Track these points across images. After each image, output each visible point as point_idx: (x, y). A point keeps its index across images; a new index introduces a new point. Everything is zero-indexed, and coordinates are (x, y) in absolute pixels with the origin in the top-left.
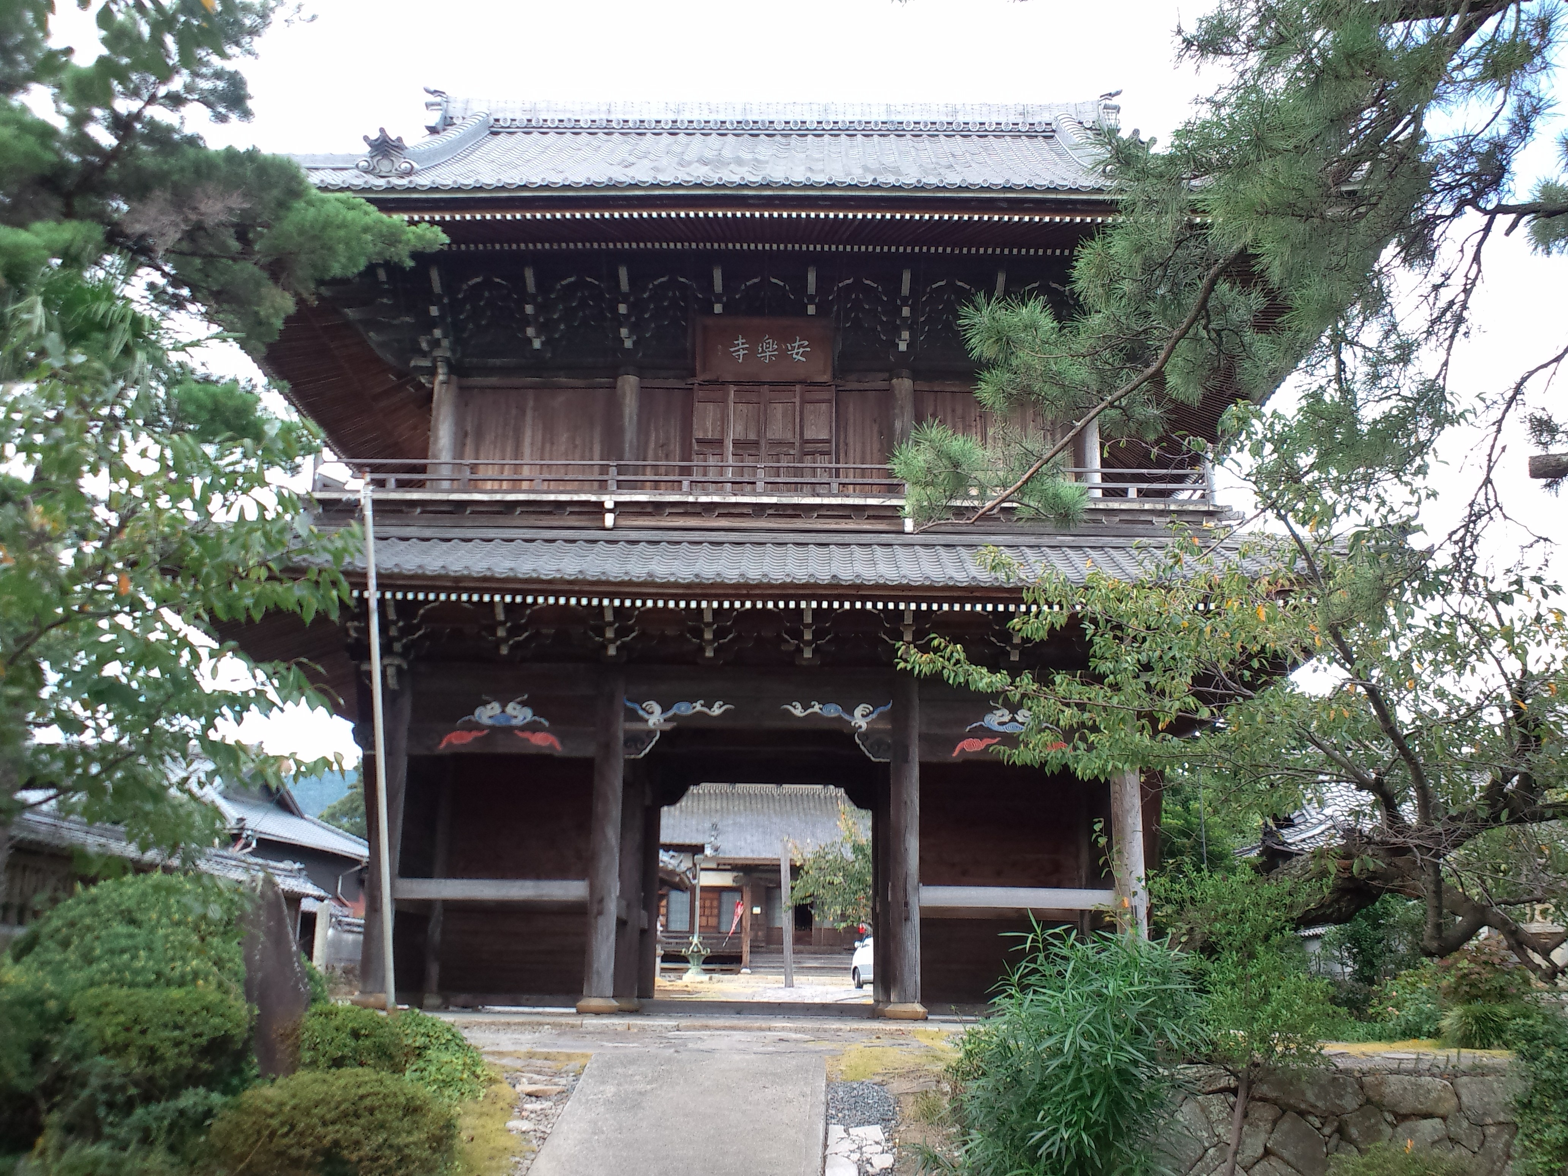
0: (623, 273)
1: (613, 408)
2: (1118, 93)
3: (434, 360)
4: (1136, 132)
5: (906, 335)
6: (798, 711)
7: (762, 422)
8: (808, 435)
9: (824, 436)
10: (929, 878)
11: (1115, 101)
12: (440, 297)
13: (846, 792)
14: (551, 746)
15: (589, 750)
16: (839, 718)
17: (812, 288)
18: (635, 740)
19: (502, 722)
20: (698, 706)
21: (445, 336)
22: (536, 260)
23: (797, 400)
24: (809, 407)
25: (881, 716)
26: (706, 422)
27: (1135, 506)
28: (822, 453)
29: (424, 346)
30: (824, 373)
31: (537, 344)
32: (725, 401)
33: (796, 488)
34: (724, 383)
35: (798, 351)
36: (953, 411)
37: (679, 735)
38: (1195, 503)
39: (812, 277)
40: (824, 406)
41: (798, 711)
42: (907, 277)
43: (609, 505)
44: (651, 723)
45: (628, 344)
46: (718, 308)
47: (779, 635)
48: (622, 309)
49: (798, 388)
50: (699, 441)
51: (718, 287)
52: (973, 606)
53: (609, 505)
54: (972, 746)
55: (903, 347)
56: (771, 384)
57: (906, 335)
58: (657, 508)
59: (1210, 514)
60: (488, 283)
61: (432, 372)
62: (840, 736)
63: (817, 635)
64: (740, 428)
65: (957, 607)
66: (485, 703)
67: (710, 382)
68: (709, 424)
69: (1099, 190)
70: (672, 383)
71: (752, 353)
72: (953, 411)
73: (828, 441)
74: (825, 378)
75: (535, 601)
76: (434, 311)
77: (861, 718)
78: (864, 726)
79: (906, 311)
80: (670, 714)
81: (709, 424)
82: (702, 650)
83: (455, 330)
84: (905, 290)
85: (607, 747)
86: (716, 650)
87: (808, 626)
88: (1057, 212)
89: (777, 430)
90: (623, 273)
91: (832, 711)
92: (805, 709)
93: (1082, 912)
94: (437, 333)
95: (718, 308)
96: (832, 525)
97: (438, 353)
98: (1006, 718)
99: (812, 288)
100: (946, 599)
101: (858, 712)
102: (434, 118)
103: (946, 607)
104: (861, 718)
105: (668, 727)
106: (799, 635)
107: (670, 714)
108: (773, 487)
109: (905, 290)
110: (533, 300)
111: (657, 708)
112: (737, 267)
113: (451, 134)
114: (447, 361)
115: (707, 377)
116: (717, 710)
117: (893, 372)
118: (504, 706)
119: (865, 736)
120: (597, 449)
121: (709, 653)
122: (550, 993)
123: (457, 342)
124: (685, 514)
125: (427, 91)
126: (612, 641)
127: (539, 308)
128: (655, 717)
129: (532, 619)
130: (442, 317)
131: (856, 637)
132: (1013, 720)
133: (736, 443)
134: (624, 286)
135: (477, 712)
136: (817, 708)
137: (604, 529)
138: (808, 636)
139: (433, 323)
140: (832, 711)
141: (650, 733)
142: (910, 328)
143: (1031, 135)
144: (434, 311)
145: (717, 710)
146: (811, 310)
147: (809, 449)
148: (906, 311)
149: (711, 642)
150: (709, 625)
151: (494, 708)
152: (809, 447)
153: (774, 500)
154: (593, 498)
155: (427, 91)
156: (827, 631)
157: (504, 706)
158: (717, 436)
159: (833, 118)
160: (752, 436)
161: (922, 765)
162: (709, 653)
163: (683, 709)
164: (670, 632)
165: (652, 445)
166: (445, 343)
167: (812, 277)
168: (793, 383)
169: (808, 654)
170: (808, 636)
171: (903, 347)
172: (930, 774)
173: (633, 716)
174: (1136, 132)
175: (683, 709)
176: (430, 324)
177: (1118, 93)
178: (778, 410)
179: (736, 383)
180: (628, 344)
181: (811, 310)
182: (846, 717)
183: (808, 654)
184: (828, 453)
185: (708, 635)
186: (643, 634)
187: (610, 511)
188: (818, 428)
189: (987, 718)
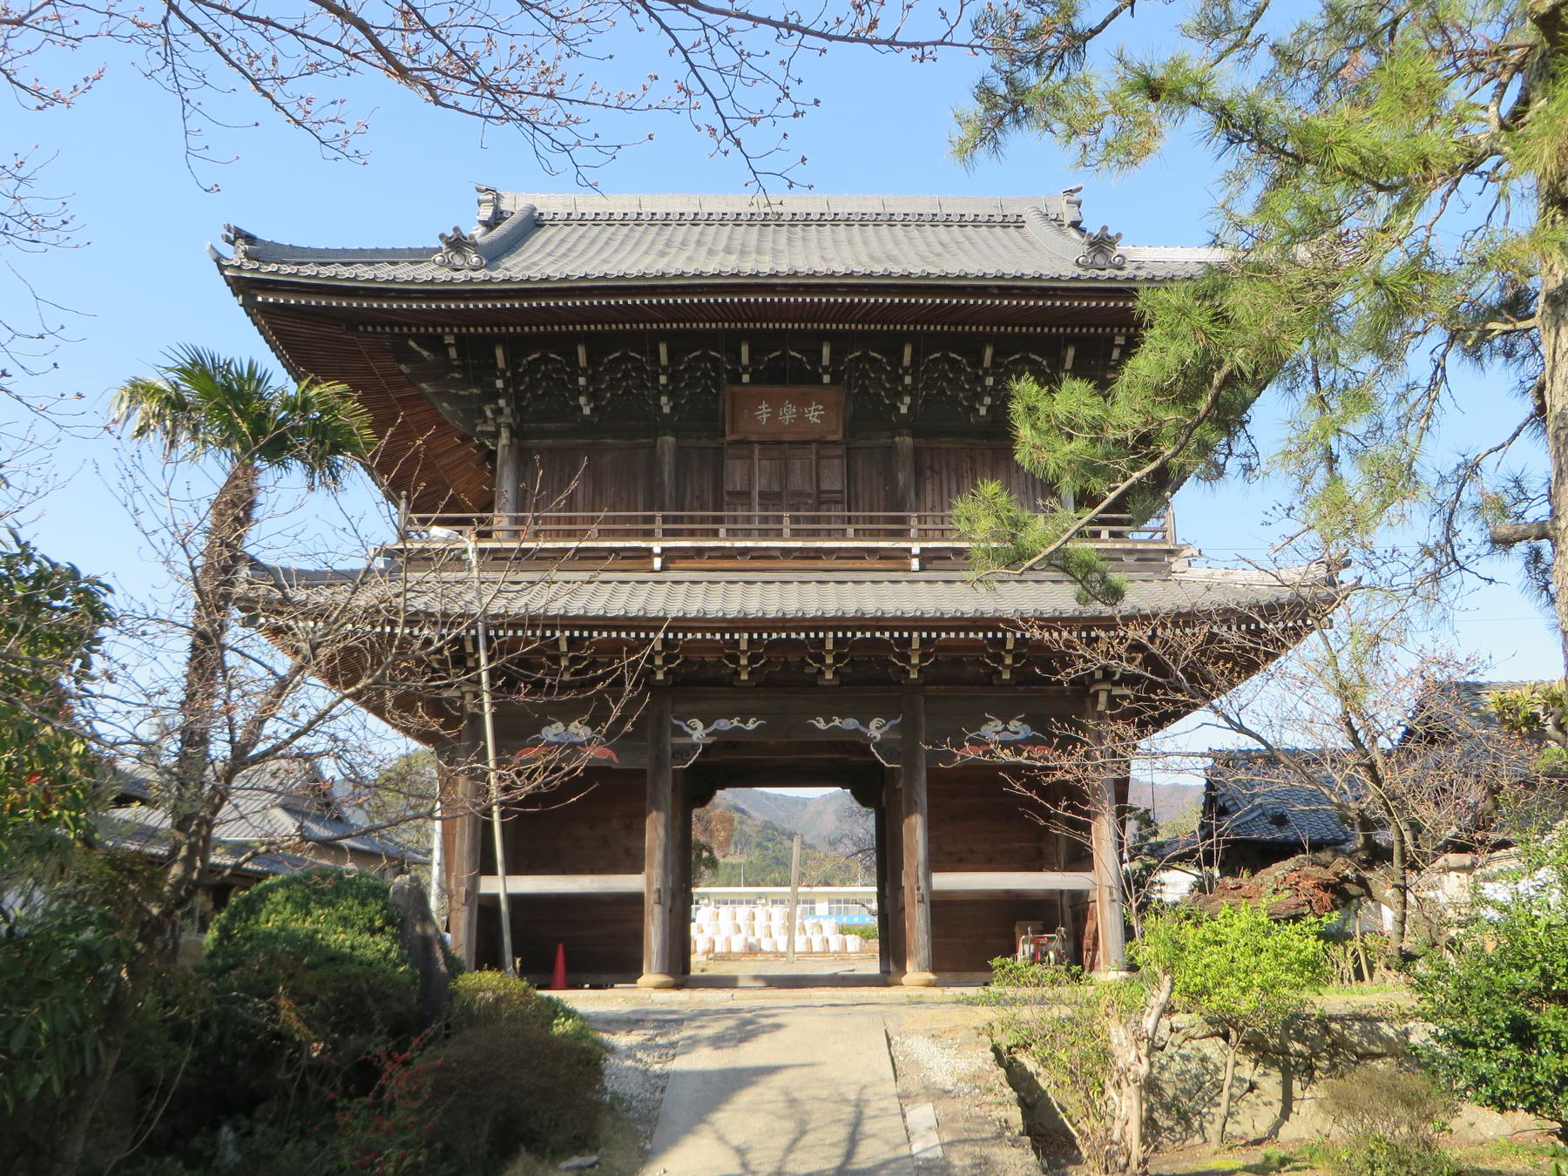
0: (663, 349)
1: (653, 464)
2: (1078, 190)
3: (498, 427)
4: (1105, 228)
5: (907, 400)
6: (821, 724)
7: (784, 475)
8: (825, 486)
9: (838, 487)
10: (636, 900)
11: (1076, 197)
12: (503, 372)
13: (853, 793)
14: (609, 760)
15: (644, 762)
16: (857, 730)
17: (826, 361)
18: (682, 752)
19: (565, 739)
20: (735, 722)
21: (508, 404)
22: (588, 339)
23: (813, 456)
24: (824, 462)
25: (893, 728)
26: (735, 475)
27: (1108, 546)
28: (836, 502)
29: (489, 414)
30: (836, 433)
31: (587, 411)
32: (751, 457)
33: (814, 534)
34: (749, 442)
35: (814, 414)
36: (948, 464)
37: (723, 743)
38: (1156, 542)
39: (826, 351)
40: (837, 462)
41: (821, 724)
42: (908, 351)
43: (657, 550)
44: (695, 738)
45: (666, 410)
46: (746, 378)
47: (803, 660)
48: (663, 379)
49: (814, 446)
50: (729, 493)
51: (745, 359)
52: (967, 634)
53: (657, 550)
54: (971, 753)
55: (904, 410)
56: (790, 443)
57: (907, 400)
58: (699, 552)
59: (1171, 552)
60: (544, 359)
61: (495, 436)
62: (858, 745)
63: (837, 659)
64: (764, 482)
65: (868, 635)
66: (550, 723)
67: (737, 442)
68: (737, 478)
69: (1077, 279)
70: (704, 443)
71: (774, 417)
72: (948, 464)
73: (842, 492)
74: (837, 437)
75: (591, 636)
76: (499, 384)
77: (875, 730)
78: (879, 737)
79: (908, 380)
80: (711, 729)
81: (737, 478)
82: (737, 673)
83: (516, 400)
84: (907, 361)
85: (659, 759)
86: (750, 674)
87: (829, 652)
88: (1039, 297)
89: (797, 481)
90: (663, 349)
91: (851, 723)
92: (827, 722)
93: (1062, 892)
94: (502, 402)
95: (746, 378)
96: (850, 564)
97: (501, 420)
98: (1000, 728)
99: (826, 361)
100: (719, 630)
101: (873, 724)
102: (486, 213)
103: (952, 635)
104: (875, 730)
105: (709, 741)
106: (821, 660)
107: (711, 729)
108: (796, 534)
109: (907, 361)
110: (584, 372)
111: (700, 725)
112: (761, 342)
113: (503, 228)
114: (509, 426)
115: (735, 437)
116: (751, 725)
117: (895, 430)
118: (566, 726)
119: (878, 746)
120: (640, 500)
121: (744, 677)
122: (933, 923)
123: (518, 410)
124: (722, 558)
125: (479, 190)
126: (660, 668)
127: (590, 380)
128: (698, 733)
129: (683, 650)
130: (505, 389)
131: (870, 660)
132: (1006, 729)
133: (762, 495)
134: (664, 360)
135: (544, 731)
136: (837, 722)
137: (653, 571)
138: (829, 660)
139: (496, 395)
140: (851, 723)
141: (694, 746)
142: (911, 394)
143: (1004, 225)
144: (499, 384)
145: (751, 725)
146: (826, 379)
147: (822, 499)
148: (908, 380)
149: (745, 667)
150: (744, 652)
151: (559, 726)
152: (824, 497)
153: (799, 544)
154: (643, 545)
155: (479, 190)
156: (760, 657)
157: (566, 726)
158: (745, 489)
159: (833, 210)
160: (776, 488)
161: (928, 770)
162: (744, 677)
163: (723, 724)
164: (709, 658)
165: (688, 497)
166: (507, 411)
167: (826, 351)
168: (809, 442)
169: (829, 676)
170: (829, 660)
171: (904, 410)
172: (935, 777)
173: (678, 731)
174: (1105, 228)
175: (723, 724)
176: (494, 395)
177: (1078, 190)
178: (797, 466)
179: (760, 443)
180: (666, 410)
181: (826, 379)
182: (862, 729)
183: (829, 676)
184: (842, 502)
185: (744, 661)
186: (686, 660)
187: (658, 555)
188: (833, 480)
189: (983, 728)
